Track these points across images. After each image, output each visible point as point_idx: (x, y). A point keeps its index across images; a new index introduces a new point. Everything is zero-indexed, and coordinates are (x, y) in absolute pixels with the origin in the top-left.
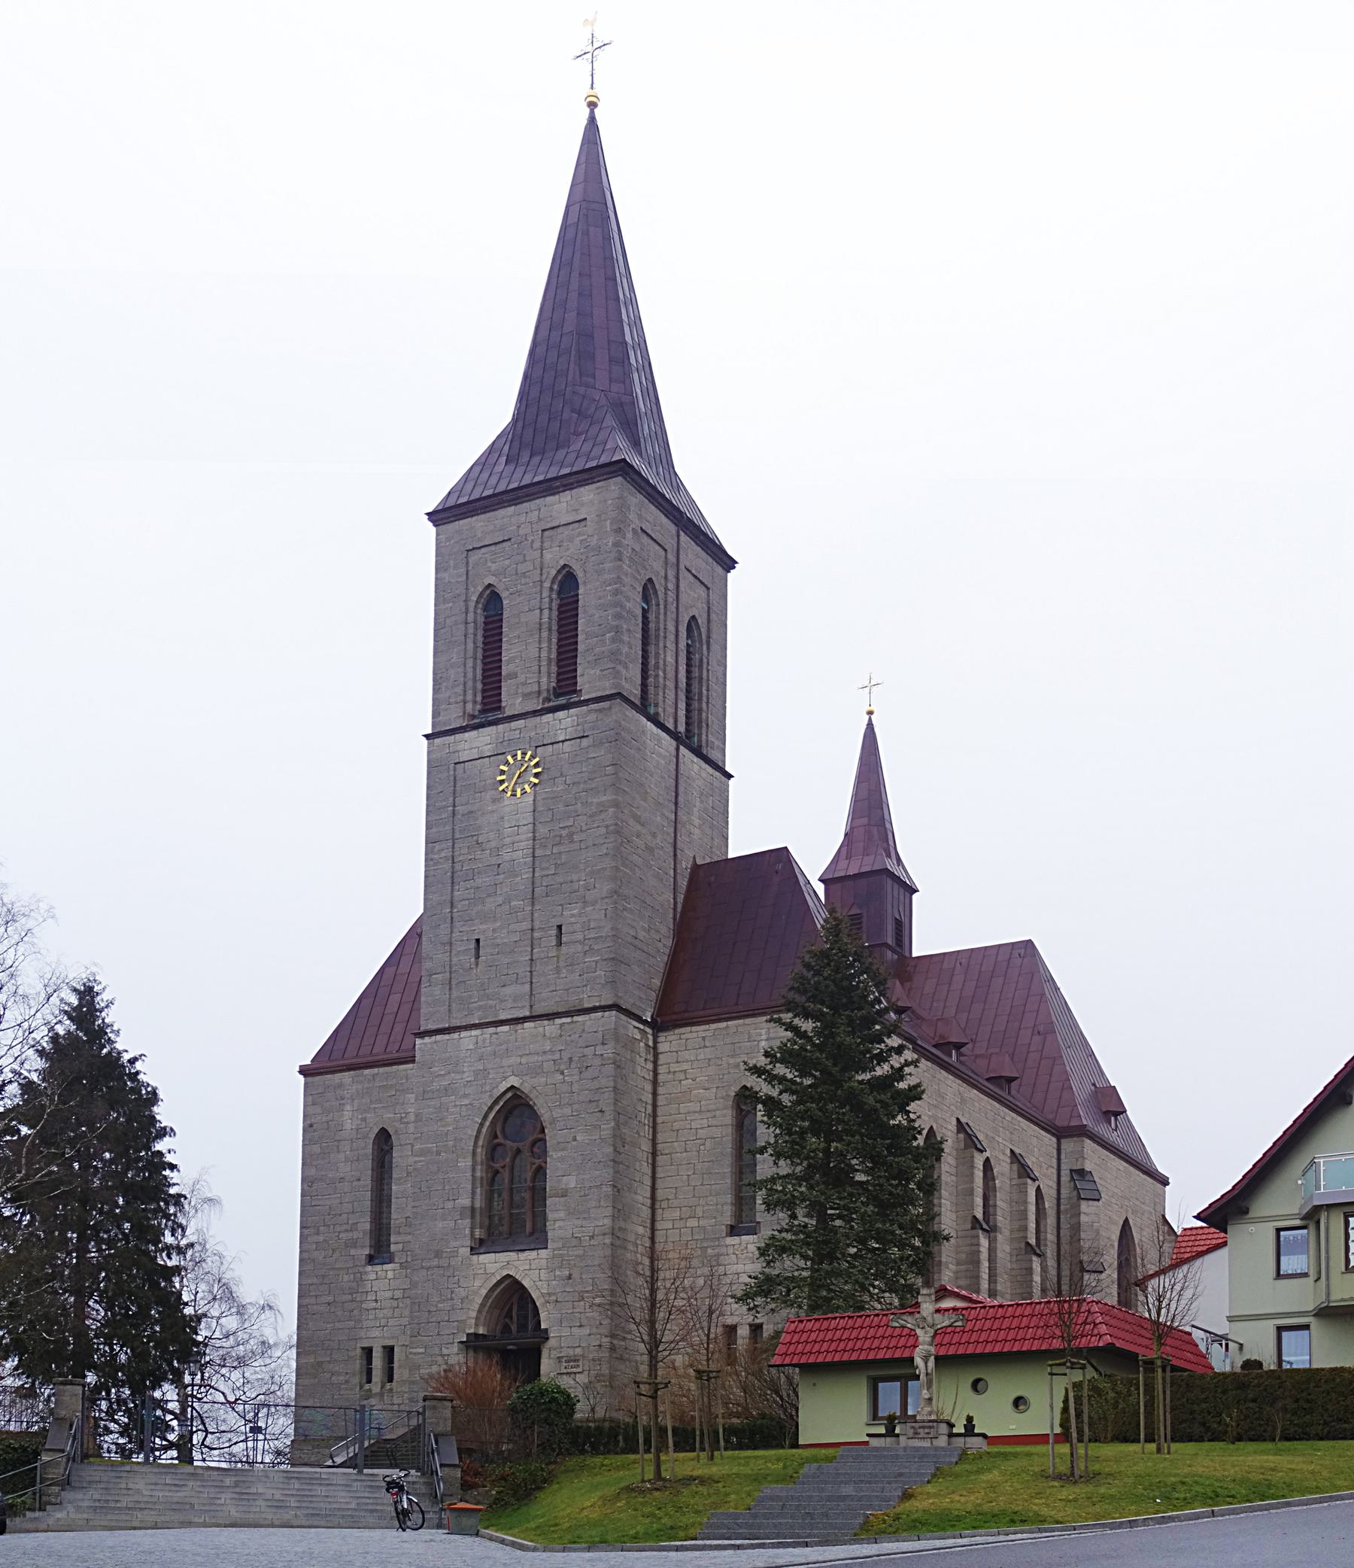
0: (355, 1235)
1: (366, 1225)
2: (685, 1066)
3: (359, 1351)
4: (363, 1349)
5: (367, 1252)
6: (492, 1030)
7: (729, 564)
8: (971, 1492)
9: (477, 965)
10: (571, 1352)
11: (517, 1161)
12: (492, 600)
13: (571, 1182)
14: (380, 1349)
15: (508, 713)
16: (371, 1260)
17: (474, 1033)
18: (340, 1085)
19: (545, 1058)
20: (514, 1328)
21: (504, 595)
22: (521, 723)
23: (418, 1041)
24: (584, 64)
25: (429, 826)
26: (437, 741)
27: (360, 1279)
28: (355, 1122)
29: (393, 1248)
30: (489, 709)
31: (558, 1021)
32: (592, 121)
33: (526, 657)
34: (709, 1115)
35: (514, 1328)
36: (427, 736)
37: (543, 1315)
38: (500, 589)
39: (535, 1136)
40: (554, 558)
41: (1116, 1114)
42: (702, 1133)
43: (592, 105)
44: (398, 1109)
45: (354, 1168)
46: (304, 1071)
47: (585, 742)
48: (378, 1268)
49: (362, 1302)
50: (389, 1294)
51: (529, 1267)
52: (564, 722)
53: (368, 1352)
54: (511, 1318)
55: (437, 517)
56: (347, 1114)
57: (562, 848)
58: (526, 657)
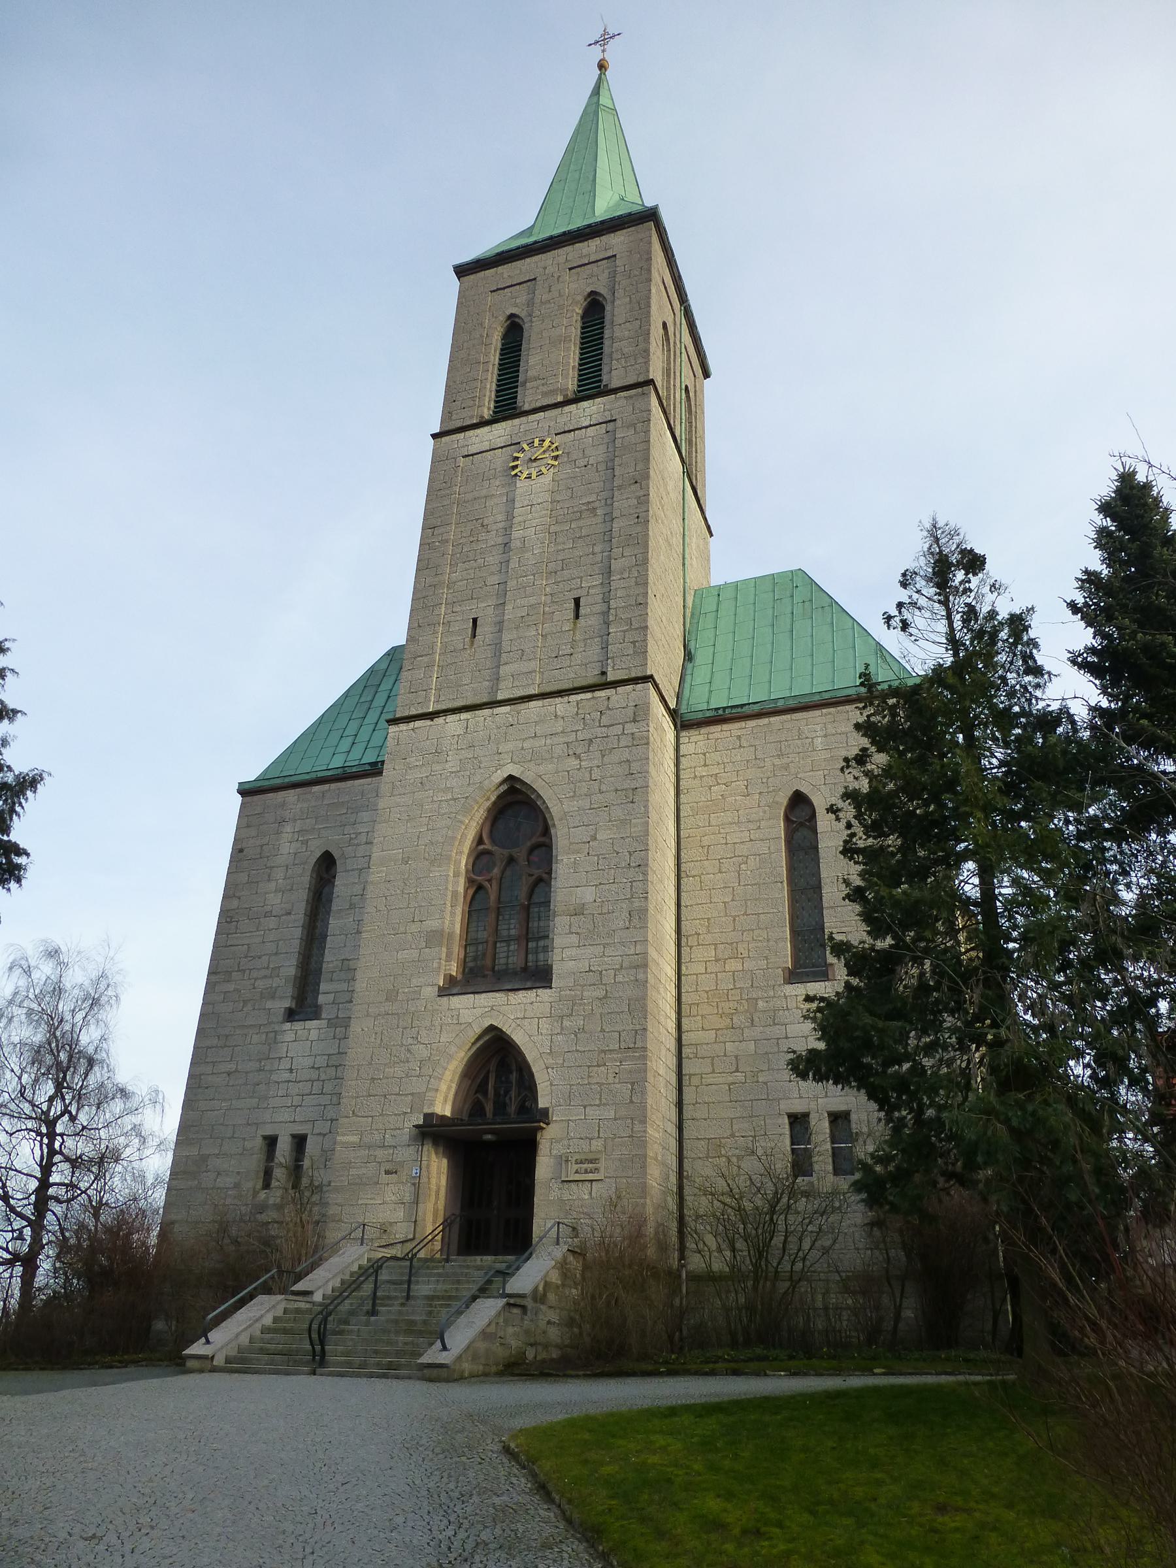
0: (276, 982)
1: (290, 969)
2: (715, 770)
3: (259, 1142)
4: (265, 1138)
5: (287, 1003)
6: (487, 712)
9: (472, 643)
10: (584, 1145)
11: (508, 873)
13: (588, 895)
14: (288, 1139)
16: (291, 1015)
17: (464, 716)
18: (283, 805)
19: (556, 740)
20: (489, 1108)
23: (393, 729)
26: (445, 439)
27: (273, 1040)
28: (293, 853)
29: (322, 999)
30: (507, 407)
31: (573, 698)
34: (751, 826)
35: (489, 1108)
36: (434, 436)
37: (542, 1088)
39: (534, 840)
42: (743, 850)
43: (602, 66)
44: (347, 829)
45: (286, 898)
46: (246, 791)
48: (298, 1025)
49: (271, 1071)
50: (308, 1062)
51: (521, 1015)
52: (591, 409)
53: (271, 1142)
54: (485, 1093)
56: (286, 837)
57: (581, 523)
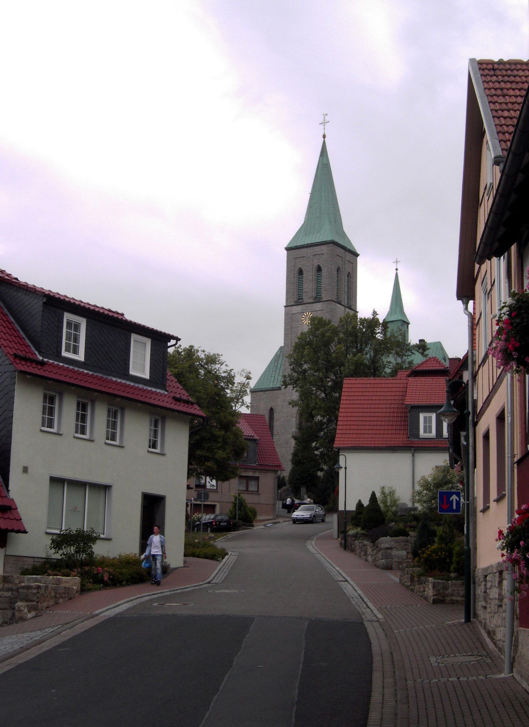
7: (357, 255)
8: (208, 467)
12: (301, 272)
15: (305, 302)
21: (304, 271)
22: (308, 305)
24: (322, 126)
25: (285, 326)
26: (287, 308)
32: (324, 142)
33: (309, 287)
38: (303, 269)
40: (316, 263)
41: (190, 545)
47: (324, 311)
55: (288, 249)
58: (309, 287)
